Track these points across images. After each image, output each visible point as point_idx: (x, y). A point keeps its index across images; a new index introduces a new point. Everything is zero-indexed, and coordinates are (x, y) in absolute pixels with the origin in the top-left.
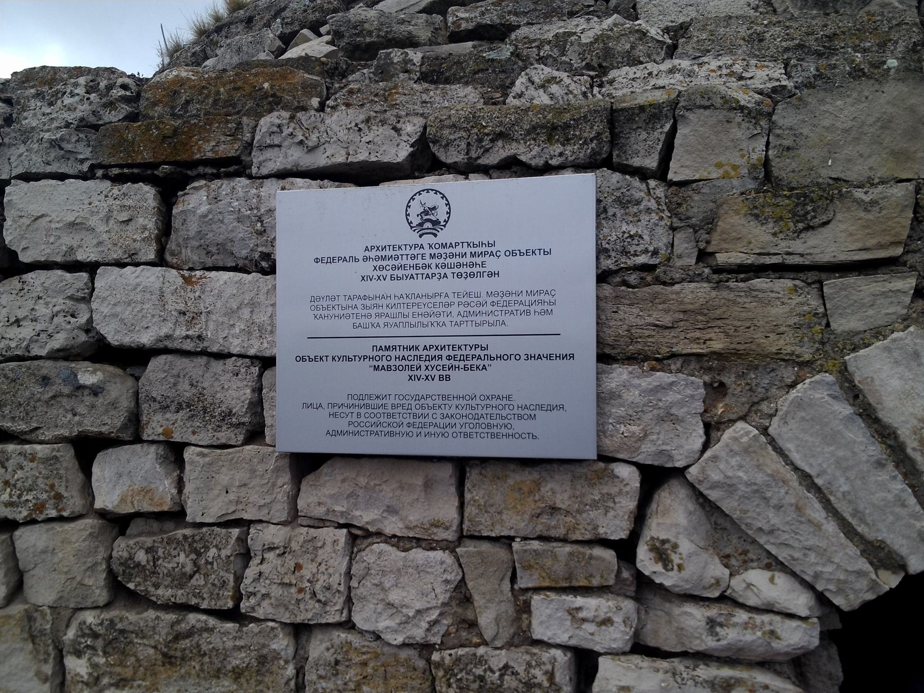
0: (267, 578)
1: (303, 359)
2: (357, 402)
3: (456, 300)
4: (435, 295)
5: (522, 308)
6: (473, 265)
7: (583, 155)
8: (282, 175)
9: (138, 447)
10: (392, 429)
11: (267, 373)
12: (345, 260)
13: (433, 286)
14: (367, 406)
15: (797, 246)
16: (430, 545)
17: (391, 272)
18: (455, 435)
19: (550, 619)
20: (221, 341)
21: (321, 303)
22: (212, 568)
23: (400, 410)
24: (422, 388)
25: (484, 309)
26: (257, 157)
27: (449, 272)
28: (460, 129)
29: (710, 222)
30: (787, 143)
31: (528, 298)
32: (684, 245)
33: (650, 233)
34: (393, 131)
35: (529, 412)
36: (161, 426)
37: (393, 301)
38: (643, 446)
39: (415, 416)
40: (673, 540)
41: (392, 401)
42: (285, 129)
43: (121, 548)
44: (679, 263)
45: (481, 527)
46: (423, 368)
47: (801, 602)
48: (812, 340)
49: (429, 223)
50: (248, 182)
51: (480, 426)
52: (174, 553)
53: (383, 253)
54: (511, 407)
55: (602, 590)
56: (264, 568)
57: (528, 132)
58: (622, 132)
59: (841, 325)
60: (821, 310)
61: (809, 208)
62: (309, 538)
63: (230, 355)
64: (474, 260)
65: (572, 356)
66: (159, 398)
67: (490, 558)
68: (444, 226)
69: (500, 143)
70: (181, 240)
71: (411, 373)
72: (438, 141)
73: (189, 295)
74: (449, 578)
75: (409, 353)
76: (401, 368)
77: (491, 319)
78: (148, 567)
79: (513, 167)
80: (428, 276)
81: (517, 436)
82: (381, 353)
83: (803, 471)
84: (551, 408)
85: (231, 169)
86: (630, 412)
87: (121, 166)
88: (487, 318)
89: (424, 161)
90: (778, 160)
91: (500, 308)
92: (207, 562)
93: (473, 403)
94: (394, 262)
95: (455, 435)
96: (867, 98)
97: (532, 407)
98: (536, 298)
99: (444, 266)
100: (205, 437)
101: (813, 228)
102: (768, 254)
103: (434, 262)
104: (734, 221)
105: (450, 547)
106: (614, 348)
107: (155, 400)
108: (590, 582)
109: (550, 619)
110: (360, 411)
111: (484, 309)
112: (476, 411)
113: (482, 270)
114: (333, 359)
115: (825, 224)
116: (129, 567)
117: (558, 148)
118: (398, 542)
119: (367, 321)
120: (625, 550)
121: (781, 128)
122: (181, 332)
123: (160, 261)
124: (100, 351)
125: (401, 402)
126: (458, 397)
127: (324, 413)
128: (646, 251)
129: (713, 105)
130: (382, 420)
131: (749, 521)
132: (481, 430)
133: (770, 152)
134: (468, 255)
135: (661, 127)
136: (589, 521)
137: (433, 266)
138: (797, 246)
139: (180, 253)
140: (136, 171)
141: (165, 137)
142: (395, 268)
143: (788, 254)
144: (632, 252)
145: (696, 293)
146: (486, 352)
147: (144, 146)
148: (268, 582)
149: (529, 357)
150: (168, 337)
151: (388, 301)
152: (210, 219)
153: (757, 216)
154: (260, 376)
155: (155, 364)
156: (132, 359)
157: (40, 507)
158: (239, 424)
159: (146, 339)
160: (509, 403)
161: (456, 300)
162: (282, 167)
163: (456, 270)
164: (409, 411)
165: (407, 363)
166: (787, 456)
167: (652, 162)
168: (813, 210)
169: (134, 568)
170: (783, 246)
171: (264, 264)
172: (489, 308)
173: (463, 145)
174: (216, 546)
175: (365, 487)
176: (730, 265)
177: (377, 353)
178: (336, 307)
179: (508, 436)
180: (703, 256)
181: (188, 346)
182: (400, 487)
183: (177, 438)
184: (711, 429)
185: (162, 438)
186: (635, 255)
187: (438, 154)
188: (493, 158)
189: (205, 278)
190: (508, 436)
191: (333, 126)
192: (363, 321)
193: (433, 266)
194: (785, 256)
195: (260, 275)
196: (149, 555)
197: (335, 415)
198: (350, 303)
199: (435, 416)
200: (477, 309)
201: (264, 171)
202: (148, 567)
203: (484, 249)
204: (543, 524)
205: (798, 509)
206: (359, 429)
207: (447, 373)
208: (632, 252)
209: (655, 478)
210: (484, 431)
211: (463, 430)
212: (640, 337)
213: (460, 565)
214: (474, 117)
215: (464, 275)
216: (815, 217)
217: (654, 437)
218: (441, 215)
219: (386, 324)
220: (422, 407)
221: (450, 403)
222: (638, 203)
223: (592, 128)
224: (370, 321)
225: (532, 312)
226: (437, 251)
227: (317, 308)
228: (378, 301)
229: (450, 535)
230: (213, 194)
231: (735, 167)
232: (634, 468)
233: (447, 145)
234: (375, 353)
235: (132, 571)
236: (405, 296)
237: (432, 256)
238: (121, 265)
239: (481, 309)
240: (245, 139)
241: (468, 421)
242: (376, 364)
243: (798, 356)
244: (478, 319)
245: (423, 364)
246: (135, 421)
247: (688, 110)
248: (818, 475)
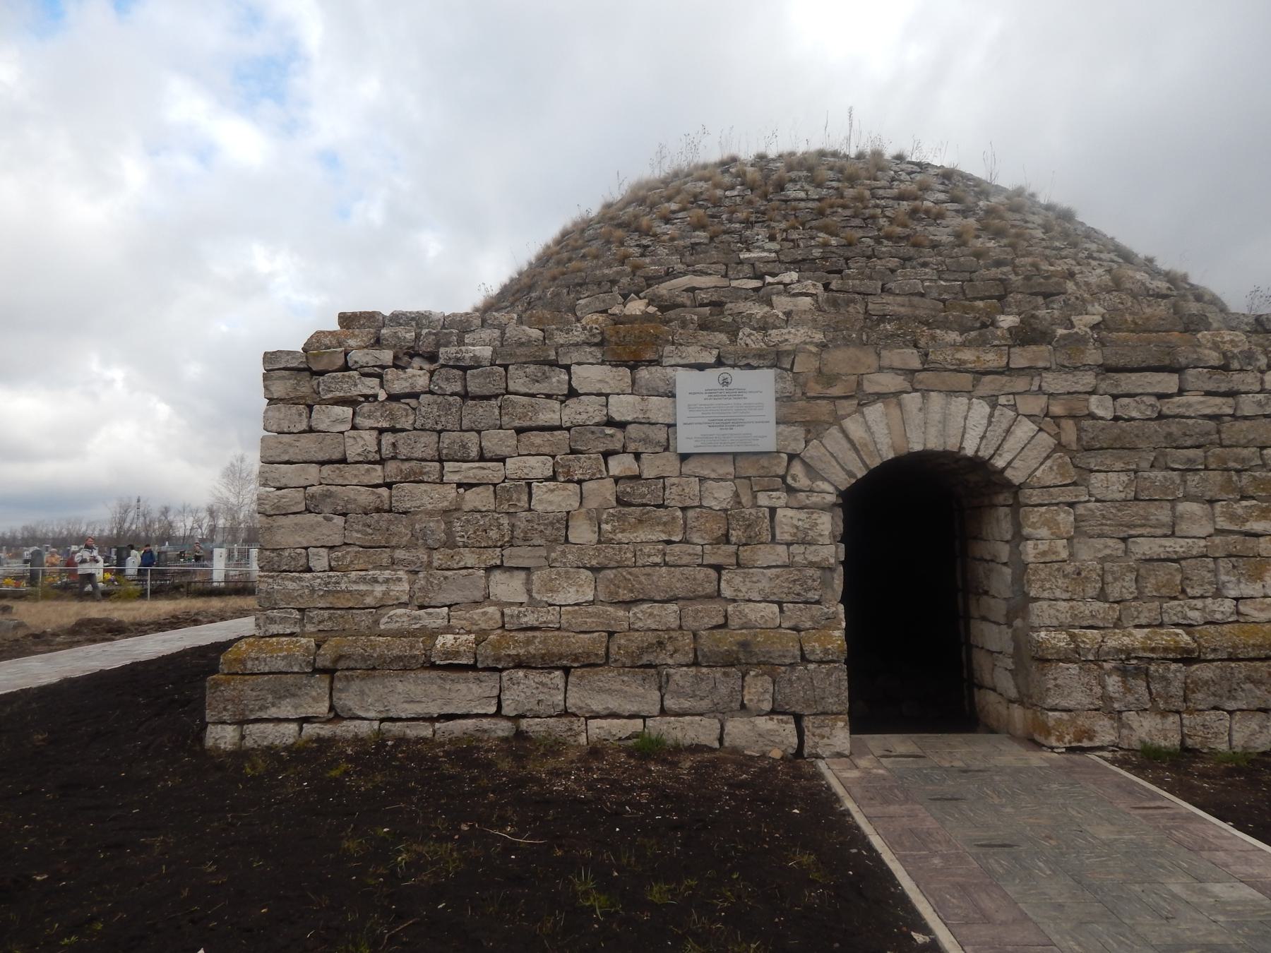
13: (728, 401)
16: (725, 480)
19: (763, 499)
24: (724, 432)
26: (664, 360)
29: (805, 384)
33: (789, 386)
43: (621, 487)
47: (831, 489)
55: (777, 490)
59: (840, 412)
79: (749, 367)
89: (719, 363)
104: (811, 384)
109: (763, 499)
120: (784, 478)
124: (610, 422)
145: (802, 404)
156: (622, 425)
157: (594, 474)
159: (629, 419)
167: (788, 367)
180: (803, 394)
184: (807, 442)
204: (762, 472)
209: (792, 457)
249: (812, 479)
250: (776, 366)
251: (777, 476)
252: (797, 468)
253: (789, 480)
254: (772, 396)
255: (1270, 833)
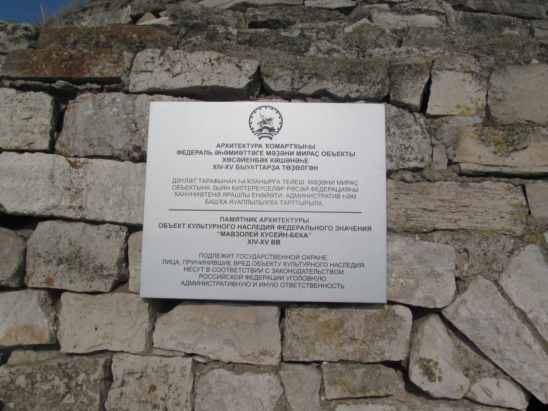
0: (127, 397)
1: (165, 226)
2: (207, 260)
3: (286, 186)
4: (269, 181)
5: (334, 193)
6: (298, 161)
7: (372, 93)
8: (152, 92)
9: (23, 293)
10: (234, 280)
11: (133, 236)
12: (201, 153)
13: (268, 174)
14: (214, 263)
15: (508, 161)
16: (257, 369)
17: (236, 163)
18: (283, 285)
20: (98, 211)
21: (181, 183)
22: (82, 389)
23: (240, 266)
25: (306, 193)
27: (280, 165)
28: (287, 68)
29: (456, 143)
30: (499, 96)
31: (338, 186)
32: (440, 157)
34: (236, 68)
35: (338, 269)
36: (44, 276)
37: (237, 184)
38: (415, 293)
39: (252, 270)
40: (435, 360)
41: (235, 259)
42: (156, 60)
44: (437, 168)
45: (299, 354)
46: (260, 234)
48: (521, 222)
49: (266, 129)
50: (125, 96)
51: (302, 279)
52: (50, 377)
53: (231, 149)
54: (325, 265)
56: (125, 389)
57: (334, 75)
58: (396, 80)
60: (525, 203)
61: (516, 138)
62: (162, 365)
63: (103, 222)
64: (299, 157)
65: (370, 228)
66: (43, 254)
67: (305, 378)
68: (278, 132)
69: (314, 80)
70: (70, 135)
71: (250, 238)
72: (270, 76)
73: (73, 175)
74: (274, 394)
75: (249, 223)
76: (242, 234)
77: (311, 200)
78: (27, 389)
80: (264, 167)
81: (330, 286)
82: (227, 223)
83: (519, 309)
84: (355, 266)
85: (114, 86)
86: (407, 269)
87: (26, 79)
88: (308, 199)
90: (493, 106)
91: (319, 193)
92: (77, 385)
93: (297, 261)
94: (239, 156)
95: (283, 285)
96: (543, 74)
97: (341, 265)
98: (345, 186)
99: (277, 160)
100: (79, 286)
101: (517, 150)
102: (492, 166)
103: (270, 157)
105: (275, 370)
106: (395, 224)
107: (40, 256)
108: (378, 392)
110: (209, 266)
111: (306, 193)
112: (299, 268)
113: (305, 164)
114: (189, 226)
115: (525, 148)
116: (10, 390)
117: (355, 87)
118: (234, 367)
119: (217, 198)
121: (494, 87)
122: (65, 202)
123: (51, 150)
125: (242, 260)
126: (286, 257)
127: (180, 268)
128: (416, 159)
129: (455, 69)
130: (226, 273)
131: (485, 344)
132: (302, 282)
133: (489, 101)
134: (295, 153)
135: (422, 79)
136: (378, 348)
137: (269, 160)
138: (508, 161)
139: (69, 144)
140: (37, 83)
141: (62, 61)
142: (239, 160)
143: (503, 166)
144: (407, 158)
145: (448, 189)
146: (307, 224)
147: (46, 65)
148: (128, 400)
149: (339, 228)
150: (54, 207)
151: (234, 184)
152: (95, 120)
153: (483, 141)
154: (127, 238)
155: (42, 227)
158: (109, 275)
160: (324, 261)
161: (286, 186)
162: (152, 86)
163: (286, 164)
164: (248, 267)
165: (247, 230)
166: (510, 299)
167: (416, 101)
168: (518, 139)
169: (14, 390)
170: (500, 162)
171: (136, 154)
172: (310, 192)
173: (289, 80)
174: (85, 372)
175: (209, 325)
176: (469, 171)
177: (224, 223)
178: (193, 187)
179: (323, 286)
181: (70, 214)
182: (236, 325)
183: (56, 285)
185: (44, 286)
186: (409, 160)
187: (269, 85)
188: (309, 90)
189: (87, 163)
190: (323, 286)
191: (193, 61)
192: (214, 198)
193: (269, 160)
194: (502, 168)
195: (131, 163)
196: (29, 380)
197: (188, 269)
198: (204, 184)
199: (267, 271)
200: (301, 193)
201: (138, 89)
202: (27, 389)
203: (306, 150)
205: (518, 334)
206: (208, 280)
207: (278, 238)
208: (407, 158)
210: (305, 282)
211: (289, 281)
212: (414, 217)
213: (282, 384)
214: (296, 62)
215: (292, 168)
216: (519, 144)
217: (424, 287)
218: (275, 124)
219: (231, 202)
220: (258, 264)
221: (279, 261)
222: (409, 127)
223: (378, 76)
224: (219, 198)
225: (342, 196)
226: (271, 150)
227: (177, 187)
228: (225, 184)
229: (274, 361)
230: (97, 103)
231: (468, 109)
232: (408, 309)
233: (276, 79)
234: (222, 223)
235: (13, 393)
236: (247, 181)
237: (268, 153)
238: (21, 151)
239: (304, 192)
240: (126, 65)
241: (293, 274)
242: (223, 231)
243: (514, 233)
244: (302, 200)
245: (259, 232)
246: (22, 272)
247: (439, 70)
248: (530, 312)
249: (472, 373)
250: (386, 100)
251: (389, 364)
252: (435, 342)
253: (417, 376)
254: (380, 165)
255: (547, 354)
